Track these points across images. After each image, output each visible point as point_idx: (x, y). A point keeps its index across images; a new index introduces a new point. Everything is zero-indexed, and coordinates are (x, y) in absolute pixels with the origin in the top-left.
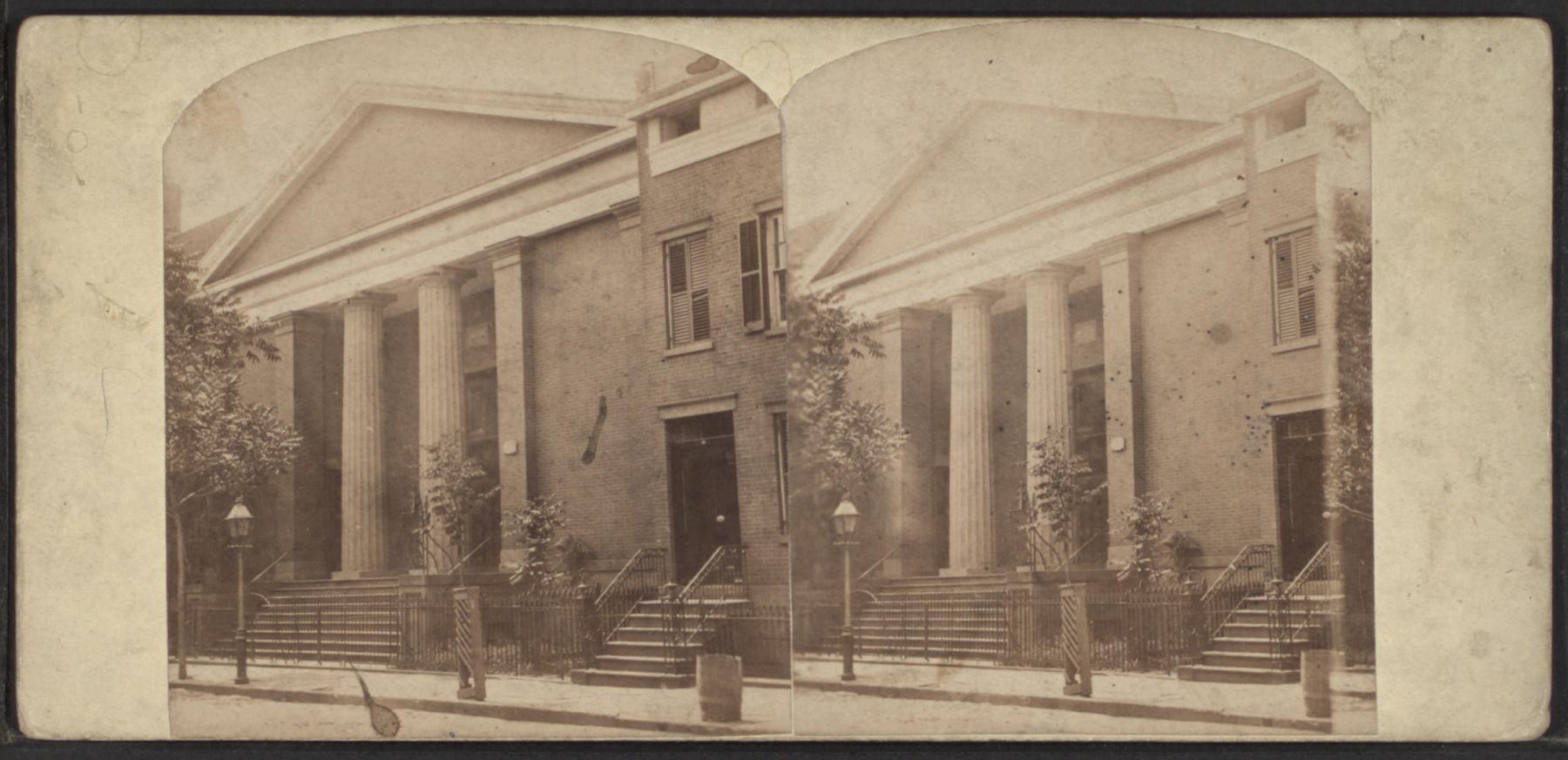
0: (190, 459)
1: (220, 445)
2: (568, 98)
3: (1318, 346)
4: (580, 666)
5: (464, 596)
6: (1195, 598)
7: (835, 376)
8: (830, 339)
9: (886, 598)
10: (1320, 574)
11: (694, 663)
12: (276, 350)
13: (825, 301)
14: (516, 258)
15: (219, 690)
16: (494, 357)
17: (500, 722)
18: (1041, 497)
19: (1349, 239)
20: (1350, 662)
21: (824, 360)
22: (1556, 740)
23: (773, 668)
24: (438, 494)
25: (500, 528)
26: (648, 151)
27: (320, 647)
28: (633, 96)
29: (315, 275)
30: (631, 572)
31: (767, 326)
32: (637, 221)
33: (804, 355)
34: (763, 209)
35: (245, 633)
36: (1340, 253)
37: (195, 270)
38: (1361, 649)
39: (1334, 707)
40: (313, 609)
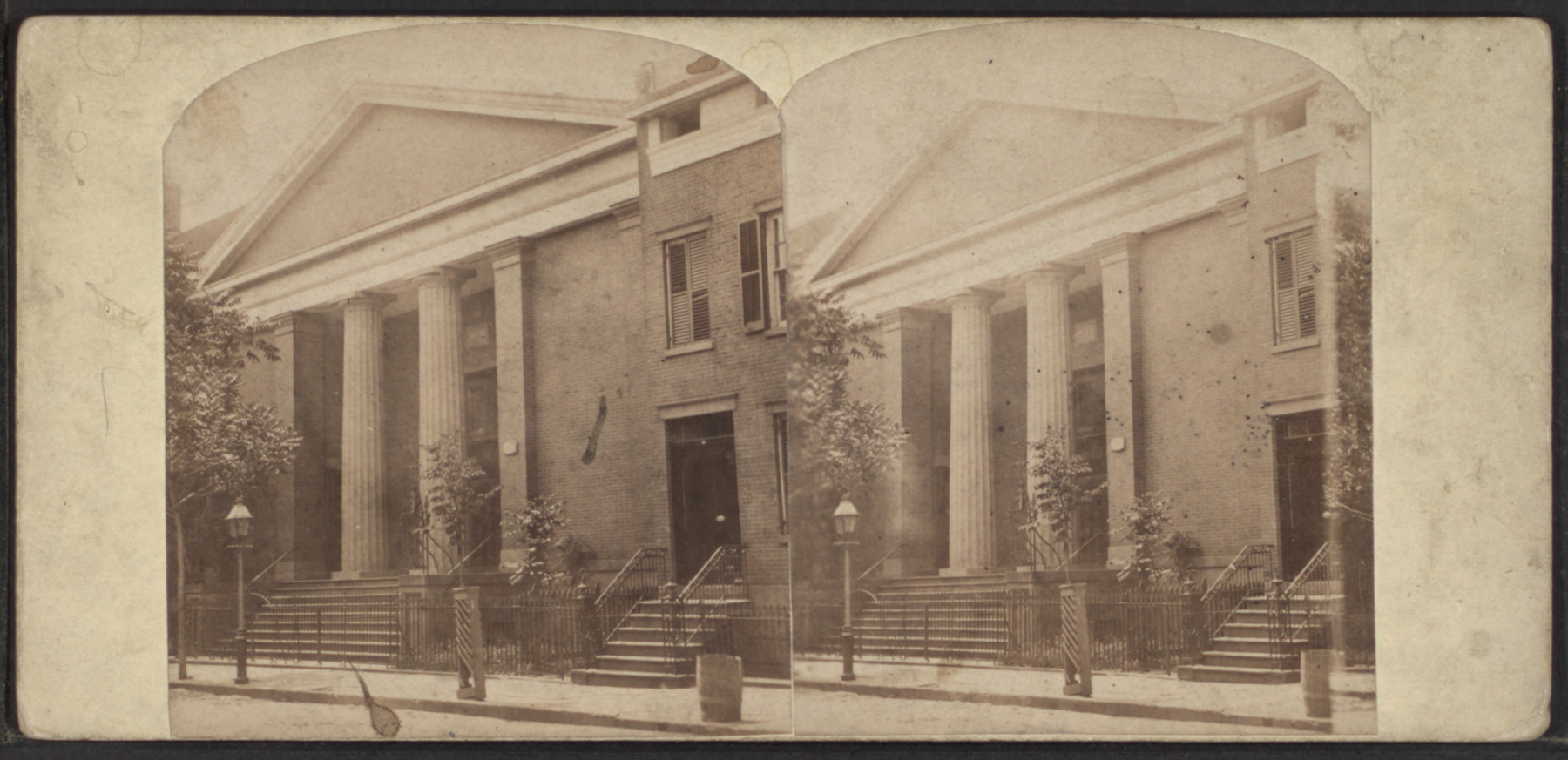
1: (220, 445)
2: (568, 98)
3: (1318, 346)
4: (580, 666)
7: (835, 376)
8: (830, 339)
10: (1320, 574)
11: (694, 663)
12: (276, 350)
13: (825, 301)
14: (516, 258)
15: (219, 690)
17: (500, 722)
18: (1041, 497)
19: (1349, 239)
20: (1349, 662)
21: (824, 360)
23: (773, 668)
25: (500, 528)
27: (320, 647)
28: (632, 95)
29: (314, 275)
30: (631, 572)
31: (767, 326)
32: (637, 221)
34: (763, 209)
35: (244, 633)
36: (1340, 253)
37: (195, 270)
38: (1361, 649)
39: (1334, 707)
40: (312, 609)
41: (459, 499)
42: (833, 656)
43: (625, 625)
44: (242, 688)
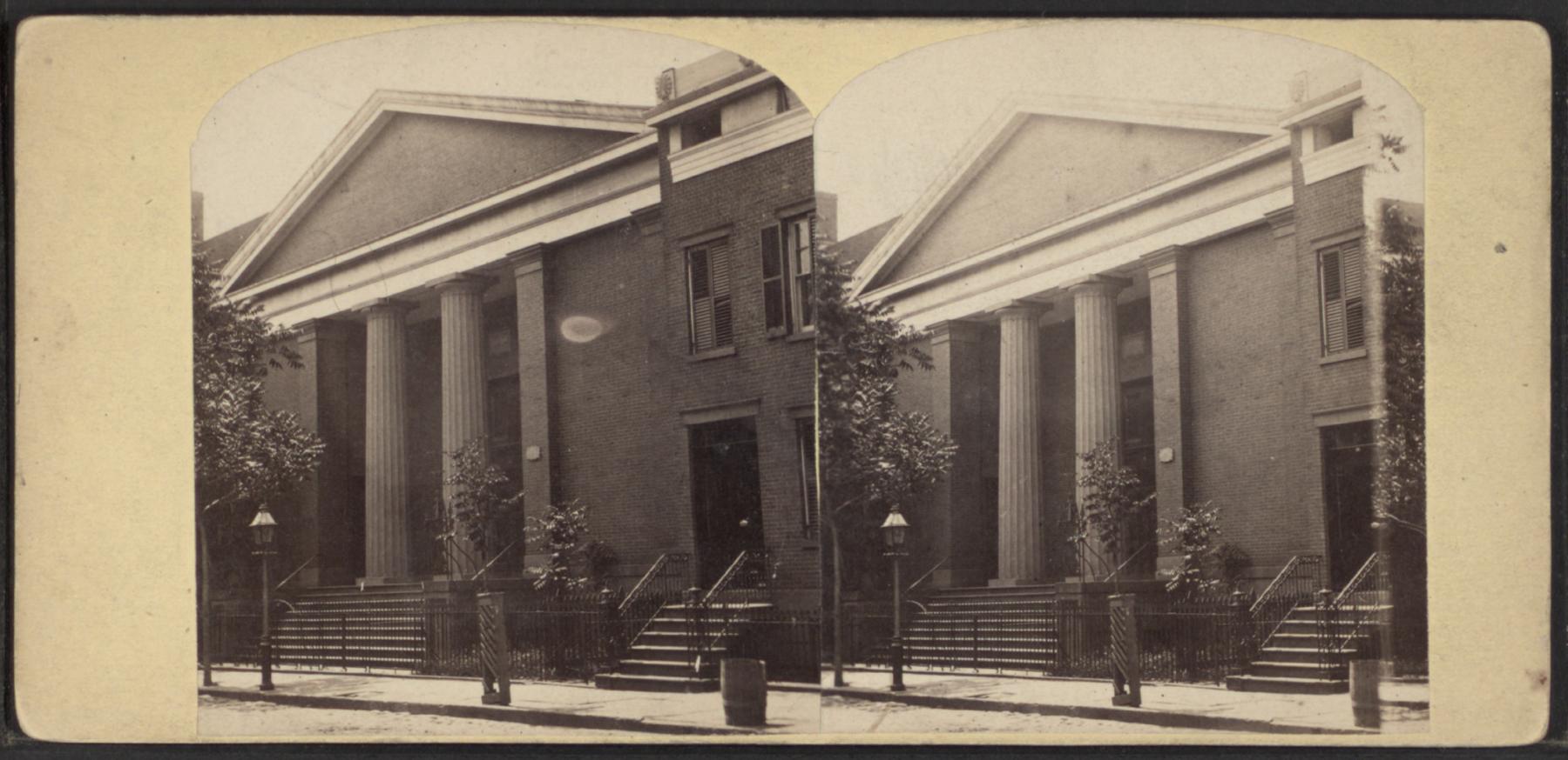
0: (213, 465)
1: (244, 452)
2: (588, 105)
3: (1366, 357)
4: (604, 671)
5: (1119, 603)
6: (612, 608)
7: (884, 388)
8: (890, 353)
9: (935, 609)
10: (1368, 584)
11: (718, 668)
12: (299, 357)
14: (538, 265)
15: (243, 696)
16: (1150, 366)
17: (526, 727)
18: (1090, 507)
19: (1395, 250)
20: (1398, 672)
21: (874, 373)
22: (1554, 742)
23: (803, 672)
26: (1302, 160)
27: (976, 654)
28: (652, 101)
29: (975, 282)
30: (1288, 577)
31: (790, 331)
32: (1291, 229)
33: (853, 366)
34: (785, 214)
35: (268, 639)
36: (1387, 265)
37: (217, 278)
38: (1413, 662)
39: (1384, 717)
40: (969, 616)
41: (1115, 507)
44: (268, 695)
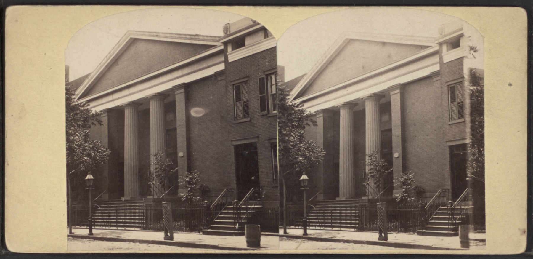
1: (83, 154)
2: (200, 36)
3: (464, 122)
4: (205, 229)
5: (380, 206)
7: (301, 132)
10: (465, 199)
11: (458, 228)
12: (101, 122)
13: (297, 107)
14: (183, 90)
15: (82, 237)
17: (179, 248)
19: (474, 85)
20: (475, 229)
21: (297, 127)
23: (273, 229)
24: (372, 171)
25: (393, 182)
28: (222, 34)
29: (331, 96)
30: (438, 197)
31: (269, 113)
32: (439, 78)
34: (267, 73)
35: (91, 218)
36: (472, 90)
37: (74, 95)
38: (480, 226)
39: (470, 244)
42: (300, 227)
43: (221, 214)
44: (91, 237)
